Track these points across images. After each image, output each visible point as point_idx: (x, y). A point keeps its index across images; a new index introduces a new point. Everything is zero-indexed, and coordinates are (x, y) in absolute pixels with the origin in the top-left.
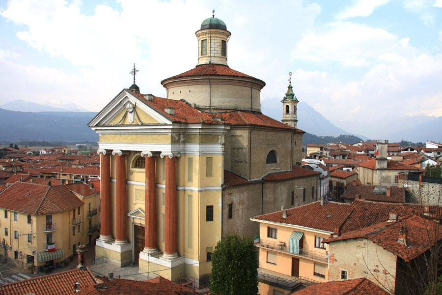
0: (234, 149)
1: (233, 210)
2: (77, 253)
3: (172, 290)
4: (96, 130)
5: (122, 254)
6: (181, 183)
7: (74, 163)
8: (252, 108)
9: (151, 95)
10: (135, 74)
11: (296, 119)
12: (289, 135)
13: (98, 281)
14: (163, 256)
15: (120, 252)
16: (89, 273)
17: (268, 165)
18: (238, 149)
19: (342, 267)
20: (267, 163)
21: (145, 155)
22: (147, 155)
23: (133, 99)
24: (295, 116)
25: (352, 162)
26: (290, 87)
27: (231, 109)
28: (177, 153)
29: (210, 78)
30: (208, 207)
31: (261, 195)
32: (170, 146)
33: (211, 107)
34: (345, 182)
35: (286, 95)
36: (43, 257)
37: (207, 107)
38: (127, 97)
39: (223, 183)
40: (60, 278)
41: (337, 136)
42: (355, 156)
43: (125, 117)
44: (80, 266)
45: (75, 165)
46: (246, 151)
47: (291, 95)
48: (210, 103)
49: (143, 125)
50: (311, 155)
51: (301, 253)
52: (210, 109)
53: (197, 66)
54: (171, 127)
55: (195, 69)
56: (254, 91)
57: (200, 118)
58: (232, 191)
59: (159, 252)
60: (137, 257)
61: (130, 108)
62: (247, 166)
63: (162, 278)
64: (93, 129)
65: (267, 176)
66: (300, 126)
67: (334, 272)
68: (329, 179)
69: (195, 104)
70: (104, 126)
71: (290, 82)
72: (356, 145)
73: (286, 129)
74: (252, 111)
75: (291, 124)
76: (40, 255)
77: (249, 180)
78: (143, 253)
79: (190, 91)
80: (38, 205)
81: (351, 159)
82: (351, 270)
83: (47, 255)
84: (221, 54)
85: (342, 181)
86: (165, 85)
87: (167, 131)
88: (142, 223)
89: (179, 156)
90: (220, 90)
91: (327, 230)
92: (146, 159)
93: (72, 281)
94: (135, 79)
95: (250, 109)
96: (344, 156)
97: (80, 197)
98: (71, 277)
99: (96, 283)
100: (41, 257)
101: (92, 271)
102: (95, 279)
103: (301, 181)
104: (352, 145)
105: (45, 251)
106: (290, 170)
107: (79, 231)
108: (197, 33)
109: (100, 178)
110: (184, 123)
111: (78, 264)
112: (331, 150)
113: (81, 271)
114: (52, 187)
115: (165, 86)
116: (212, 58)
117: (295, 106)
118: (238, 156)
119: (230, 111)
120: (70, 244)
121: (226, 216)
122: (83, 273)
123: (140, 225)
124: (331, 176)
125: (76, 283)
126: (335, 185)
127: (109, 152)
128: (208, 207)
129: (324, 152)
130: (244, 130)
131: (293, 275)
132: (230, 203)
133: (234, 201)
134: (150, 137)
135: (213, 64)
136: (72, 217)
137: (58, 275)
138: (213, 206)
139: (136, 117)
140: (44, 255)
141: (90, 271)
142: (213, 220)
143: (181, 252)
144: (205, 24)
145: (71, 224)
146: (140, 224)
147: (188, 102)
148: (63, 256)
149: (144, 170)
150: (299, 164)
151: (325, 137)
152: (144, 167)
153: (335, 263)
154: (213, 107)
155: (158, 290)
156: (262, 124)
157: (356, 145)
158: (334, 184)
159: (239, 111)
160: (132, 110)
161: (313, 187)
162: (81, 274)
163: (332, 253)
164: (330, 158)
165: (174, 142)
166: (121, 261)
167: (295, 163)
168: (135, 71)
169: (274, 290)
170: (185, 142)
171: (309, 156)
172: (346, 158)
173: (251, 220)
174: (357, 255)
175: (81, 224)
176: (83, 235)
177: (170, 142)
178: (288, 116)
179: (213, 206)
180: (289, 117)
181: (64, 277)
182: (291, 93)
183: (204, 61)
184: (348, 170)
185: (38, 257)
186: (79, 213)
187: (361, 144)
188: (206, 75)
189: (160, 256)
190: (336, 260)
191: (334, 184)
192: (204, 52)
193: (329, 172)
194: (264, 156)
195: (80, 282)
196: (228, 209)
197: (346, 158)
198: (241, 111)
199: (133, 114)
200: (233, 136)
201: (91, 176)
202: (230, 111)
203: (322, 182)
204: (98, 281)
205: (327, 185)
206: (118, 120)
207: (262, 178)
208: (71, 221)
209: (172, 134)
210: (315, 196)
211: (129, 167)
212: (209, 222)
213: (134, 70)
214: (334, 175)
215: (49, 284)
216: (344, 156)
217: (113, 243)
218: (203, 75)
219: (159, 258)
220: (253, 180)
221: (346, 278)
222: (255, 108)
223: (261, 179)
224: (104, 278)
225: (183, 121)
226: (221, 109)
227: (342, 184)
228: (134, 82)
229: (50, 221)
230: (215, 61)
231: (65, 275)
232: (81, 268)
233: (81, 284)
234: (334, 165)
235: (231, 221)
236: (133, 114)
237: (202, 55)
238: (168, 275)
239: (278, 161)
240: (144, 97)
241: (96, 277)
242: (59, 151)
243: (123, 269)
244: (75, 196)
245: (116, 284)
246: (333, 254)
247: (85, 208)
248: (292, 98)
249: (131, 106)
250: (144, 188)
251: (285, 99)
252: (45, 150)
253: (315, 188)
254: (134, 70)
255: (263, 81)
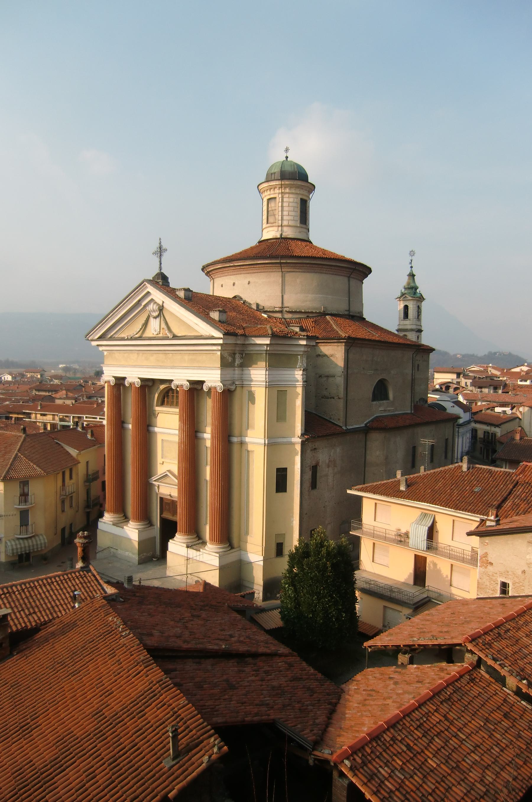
0: (320, 376)
1: (318, 475)
2: (76, 544)
3: (224, 604)
4: (98, 345)
5: (141, 543)
6: (236, 431)
7: (58, 395)
8: (349, 311)
9: (187, 290)
10: (161, 255)
11: (419, 327)
12: (409, 354)
13: (110, 590)
14: (129, 525)
15: (218, 565)
16: (94, 576)
17: (375, 403)
18: (328, 377)
19: (501, 574)
20: (373, 400)
21: (177, 387)
22: (182, 386)
23: (158, 296)
24: (418, 323)
25: (509, 397)
26: (412, 276)
27: (316, 313)
28: (230, 382)
29: (282, 261)
30: (278, 470)
31: (364, 452)
32: (219, 372)
33: (285, 309)
34: (498, 431)
35: (405, 288)
36: (14, 547)
37: (277, 309)
38: (148, 292)
39: (303, 432)
40: (50, 585)
41: (483, 354)
42: (516, 388)
43: (146, 324)
44: (79, 565)
45: (60, 398)
46: (340, 381)
47: (412, 288)
48: (282, 303)
49: (175, 337)
50: (441, 385)
51: (429, 548)
52: (281, 312)
53: (260, 242)
54: (221, 341)
55: (256, 247)
56: (353, 282)
57: (268, 327)
58: (318, 444)
59: (200, 541)
60: (164, 548)
61: (154, 311)
62: (341, 404)
63: (206, 585)
64: (94, 343)
65: (372, 421)
66: (426, 340)
67: (488, 584)
68: (473, 425)
69: (258, 305)
70: (111, 339)
71: (412, 267)
72: (517, 370)
73: (404, 345)
74: (349, 315)
75: (412, 337)
76: (9, 544)
77: (344, 428)
78: (204, 551)
79: (249, 283)
80: (7, 465)
81: (508, 392)
82: (517, 581)
83: (20, 544)
84: (299, 222)
85: (493, 429)
86: (208, 272)
87: (215, 348)
88: (172, 494)
89: (233, 388)
90: (298, 281)
91: (473, 511)
92: (180, 393)
93: (68, 589)
94: (161, 264)
95: (346, 313)
96: (496, 388)
97: (73, 452)
98: (67, 582)
99: (106, 592)
100: (10, 548)
101: (99, 573)
102: (105, 586)
103: (426, 429)
104: (511, 369)
105: (18, 539)
106: (409, 412)
107: (71, 506)
108: (260, 187)
109: (105, 422)
110: (241, 335)
111: (77, 562)
112: (475, 378)
113: (81, 573)
114: (27, 436)
115: (208, 274)
116: (285, 229)
117: (418, 307)
118: (326, 389)
119: (314, 315)
120: (56, 527)
121: (308, 484)
122: (85, 576)
123: (169, 497)
124: (476, 422)
125: (76, 593)
126: (482, 436)
127: (120, 381)
128: (278, 470)
129: (463, 381)
130: (338, 346)
131: (415, 583)
132: (314, 463)
133: (320, 461)
134: (186, 357)
135: (286, 239)
136: (60, 483)
137: (46, 579)
138: (286, 469)
139: (163, 325)
140: (16, 545)
141: (96, 574)
142: (286, 491)
143: (235, 542)
144: (273, 171)
145: (58, 496)
146: (170, 495)
147: (247, 300)
148: (45, 547)
149: (177, 410)
150: (425, 400)
151: (464, 356)
152: (177, 405)
153: (490, 568)
154: (287, 309)
155: (202, 604)
156: (367, 337)
157: (517, 370)
158: (480, 435)
159: (328, 314)
160: (157, 314)
161: (447, 440)
162: (82, 578)
163: (485, 551)
164: (472, 391)
165: (225, 364)
166: (139, 555)
167: (418, 400)
168: (160, 251)
169: (385, 607)
170: (242, 366)
171: (437, 387)
172: (500, 391)
173: (349, 492)
174: (528, 557)
175: (74, 495)
176: (77, 511)
177: (219, 365)
178: (407, 322)
179: (286, 469)
180: (408, 324)
181: (55, 584)
182: (412, 285)
183: (270, 233)
184: (504, 412)
185: (6, 547)
186: (71, 478)
187: (525, 369)
188: (276, 257)
189: (125, 525)
190: (491, 564)
191: (480, 435)
192: (271, 220)
193: (472, 413)
194: (368, 388)
195: (81, 591)
196: (311, 472)
197: (500, 391)
198: (332, 315)
199: (158, 319)
200: (319, 355)
201: (86, 417)
202: (314, 315)
203: (461, 430)
204: (110, 590)
205: (469, 435)
206: (135, 329)
207: (366, 425)
208: (58, 491)
209: (223, 352)
210: (449, 455)
211: (151, 406)
212: (280, 494)
213: (160, 248)
214: (479, 419)
215: (33, 594)
216: (496, 388)
217: (127, 525)
218: (271, 257)
219: (199, 551)
220: (351, 427)
221: (508, 593)
222: (354, 309)
223: (363, 425)
224: (117, 585)
225: (240, 332)
226: (300, 312)
227: (494, 435)
228: (160, 268)
229: (26, 490)
230: (289, 233)
231: (57, 579)
232: (81, 568)
233: (83, 593)
234: (479, 404)
235: (315, 492)
236: (158, 320)
237: (267, 223)
238: (214, 579)
239: (391, 396)
240: (177, 293)
241: (106, 582)
242: (32, 377)
243: (141, 566)
244: (65, 449)
245: (138, 594)
246: (486, 553)
247: (81, 470)
248: (415, 293)
249: (155, 307)
250: (176, 439)
251: (403, 294)
252: (10, 374)
253: (450, 441)
254: (160, 248)
255: (368, 265)
